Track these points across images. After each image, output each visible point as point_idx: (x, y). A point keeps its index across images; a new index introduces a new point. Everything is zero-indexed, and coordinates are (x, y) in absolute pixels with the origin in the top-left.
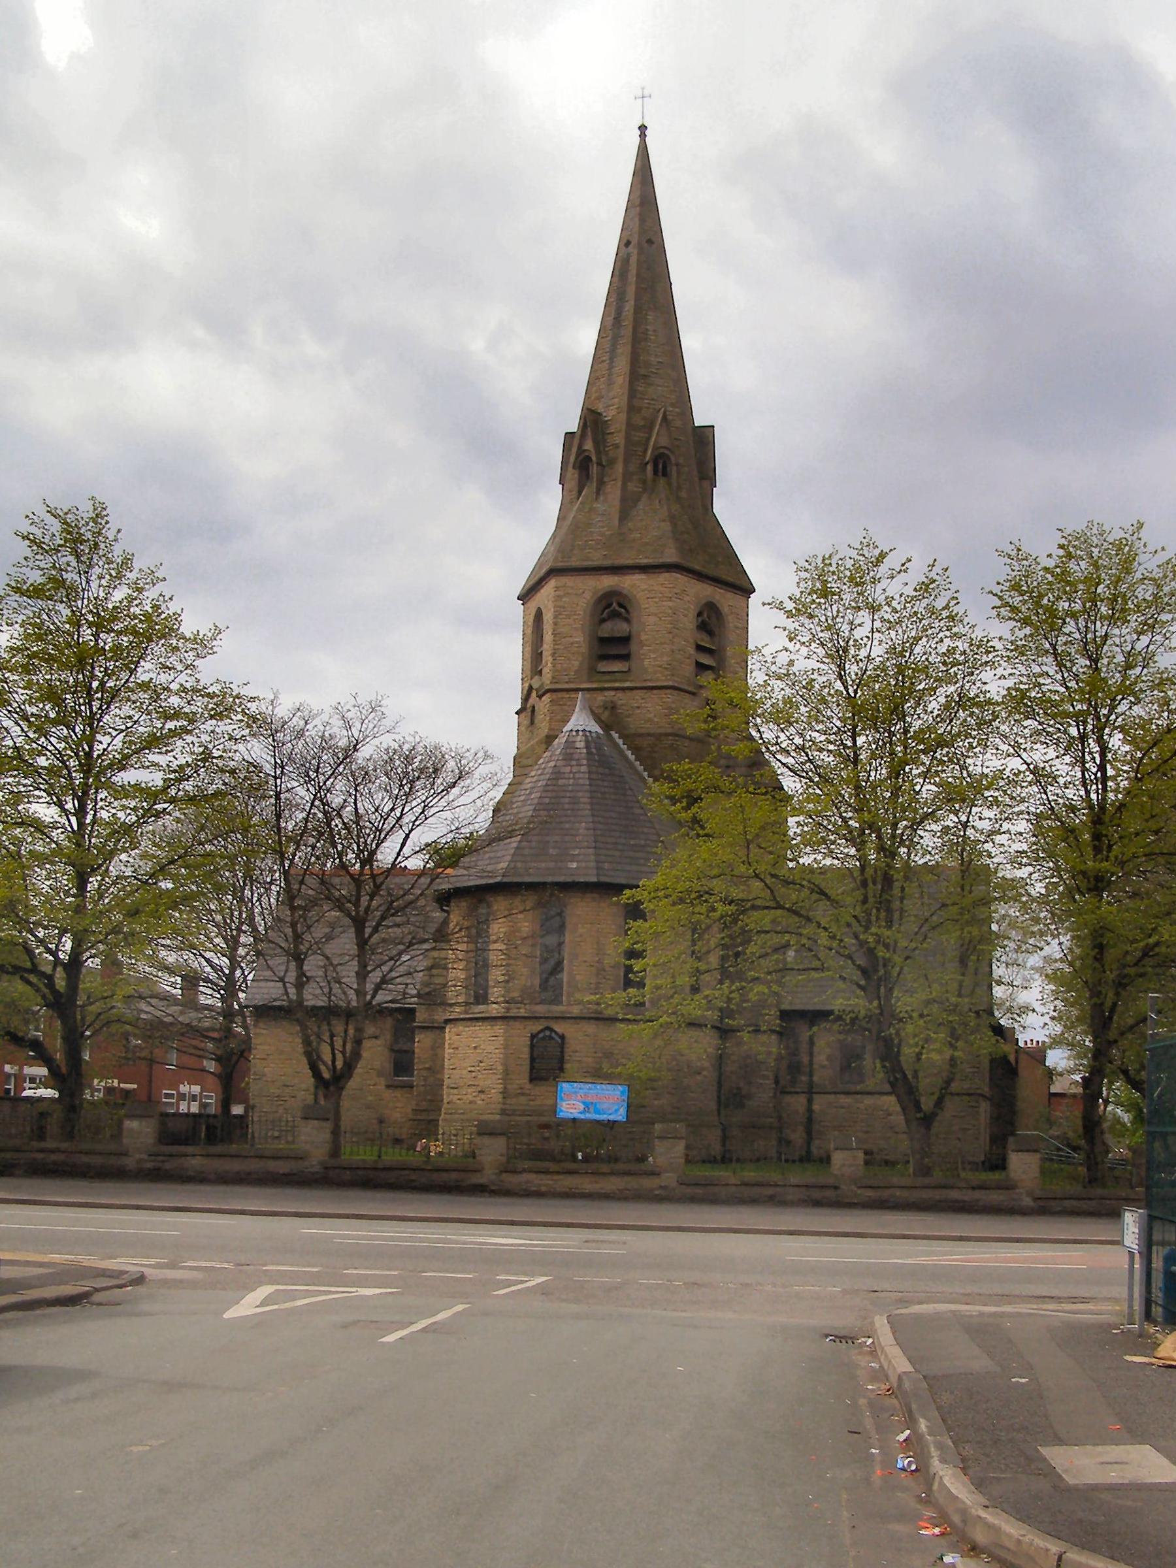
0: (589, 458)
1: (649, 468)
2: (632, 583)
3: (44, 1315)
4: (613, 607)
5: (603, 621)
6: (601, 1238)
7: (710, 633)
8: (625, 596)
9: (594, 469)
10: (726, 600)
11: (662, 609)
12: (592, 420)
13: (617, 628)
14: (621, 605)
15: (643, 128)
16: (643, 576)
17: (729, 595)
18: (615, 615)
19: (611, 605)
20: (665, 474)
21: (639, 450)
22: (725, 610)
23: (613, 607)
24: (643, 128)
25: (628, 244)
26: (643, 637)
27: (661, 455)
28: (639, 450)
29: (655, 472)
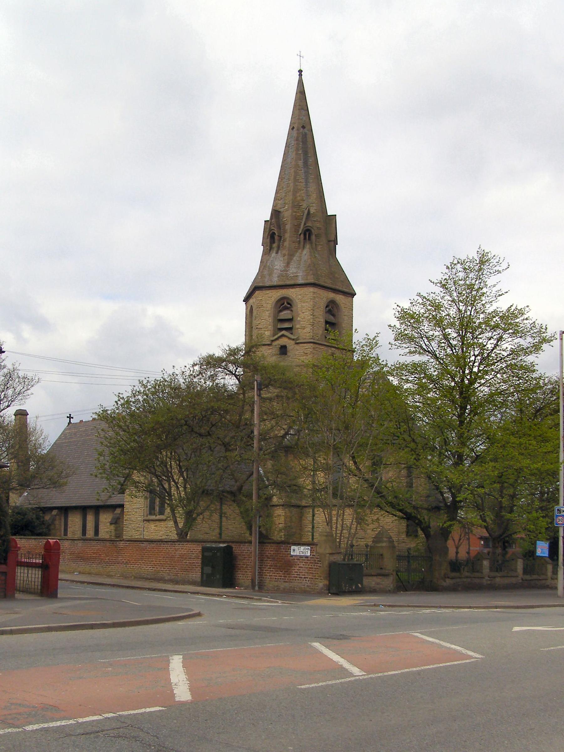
0: (274, 233)
1: (302, 236)
2: (291, 293)
3: (271, 631)
4: (285, 304)
5: (281, 311)
6: (270, 620)
7: (333, 315)
8: (291, 300)
9: (276, 237)
10: (339, 298)
11: (307, 307)
12: (276, 213)
13: (285, 314)
14: (289, 304)
15: (300, 71)
16: (343, 297)
17: (291, 290)
18: (286, 308)
19: (284, 304)
20: (309, 239)
21: (301, 227)
22: (342, 306)
23: (285, 304)
24: (300, 71)
25: (293, 128)
26: (343, 326)
27: (308, 230)
28: (301, 227)
29: (305, 239)
